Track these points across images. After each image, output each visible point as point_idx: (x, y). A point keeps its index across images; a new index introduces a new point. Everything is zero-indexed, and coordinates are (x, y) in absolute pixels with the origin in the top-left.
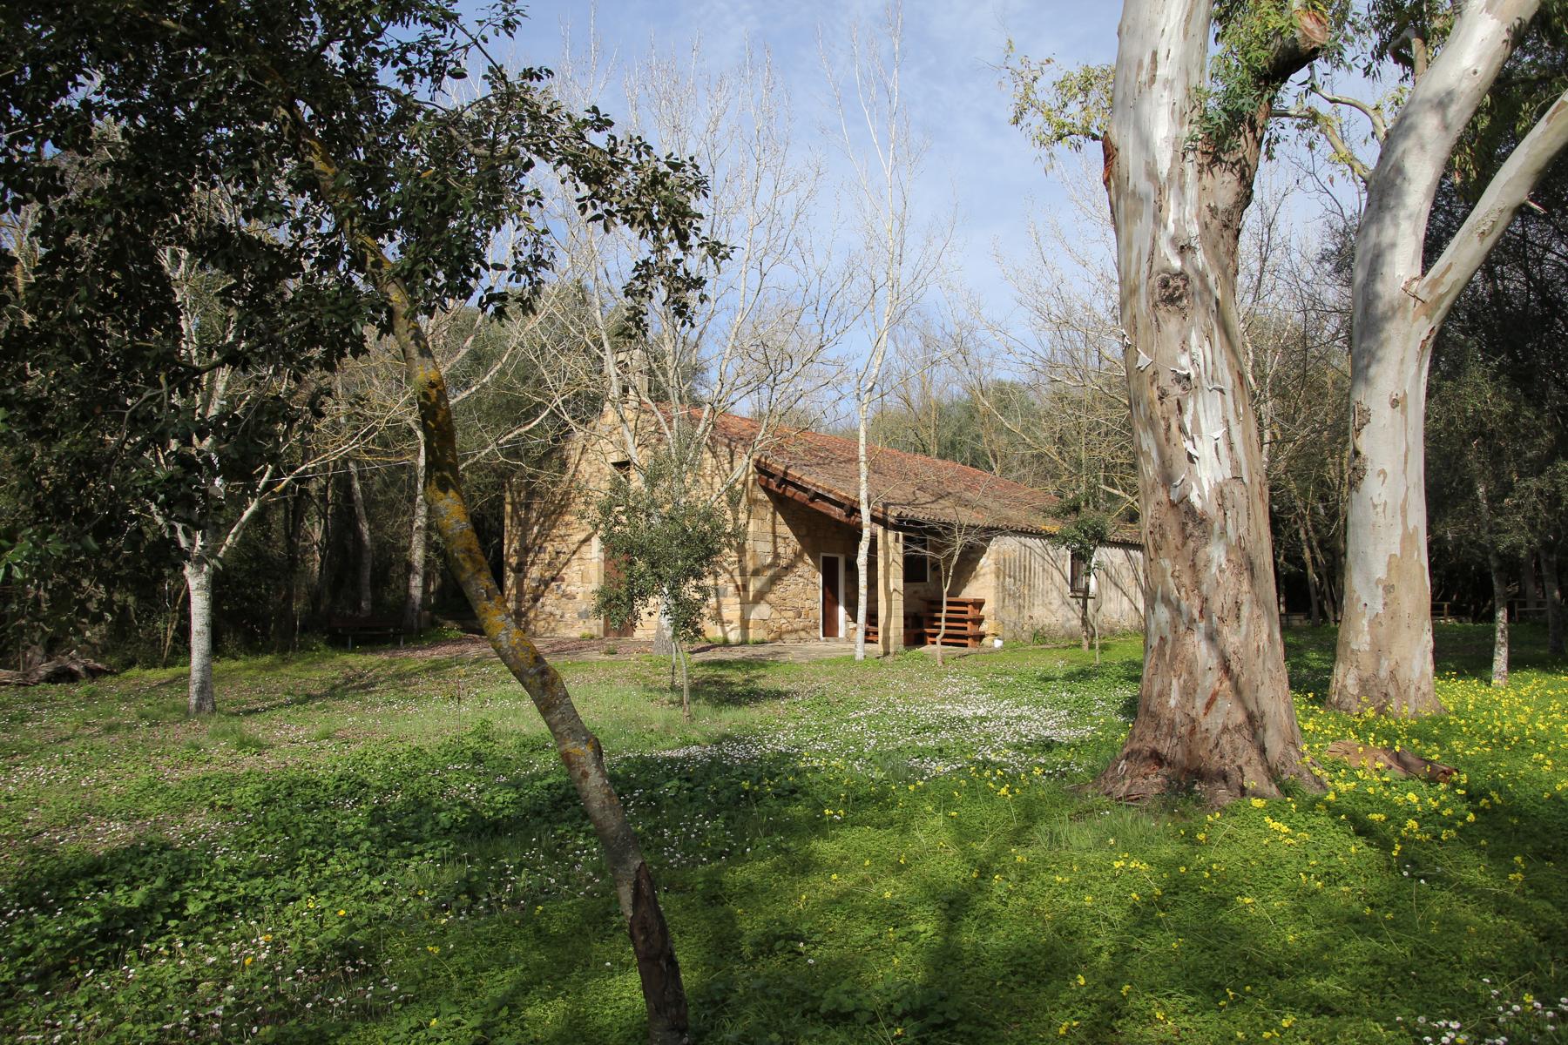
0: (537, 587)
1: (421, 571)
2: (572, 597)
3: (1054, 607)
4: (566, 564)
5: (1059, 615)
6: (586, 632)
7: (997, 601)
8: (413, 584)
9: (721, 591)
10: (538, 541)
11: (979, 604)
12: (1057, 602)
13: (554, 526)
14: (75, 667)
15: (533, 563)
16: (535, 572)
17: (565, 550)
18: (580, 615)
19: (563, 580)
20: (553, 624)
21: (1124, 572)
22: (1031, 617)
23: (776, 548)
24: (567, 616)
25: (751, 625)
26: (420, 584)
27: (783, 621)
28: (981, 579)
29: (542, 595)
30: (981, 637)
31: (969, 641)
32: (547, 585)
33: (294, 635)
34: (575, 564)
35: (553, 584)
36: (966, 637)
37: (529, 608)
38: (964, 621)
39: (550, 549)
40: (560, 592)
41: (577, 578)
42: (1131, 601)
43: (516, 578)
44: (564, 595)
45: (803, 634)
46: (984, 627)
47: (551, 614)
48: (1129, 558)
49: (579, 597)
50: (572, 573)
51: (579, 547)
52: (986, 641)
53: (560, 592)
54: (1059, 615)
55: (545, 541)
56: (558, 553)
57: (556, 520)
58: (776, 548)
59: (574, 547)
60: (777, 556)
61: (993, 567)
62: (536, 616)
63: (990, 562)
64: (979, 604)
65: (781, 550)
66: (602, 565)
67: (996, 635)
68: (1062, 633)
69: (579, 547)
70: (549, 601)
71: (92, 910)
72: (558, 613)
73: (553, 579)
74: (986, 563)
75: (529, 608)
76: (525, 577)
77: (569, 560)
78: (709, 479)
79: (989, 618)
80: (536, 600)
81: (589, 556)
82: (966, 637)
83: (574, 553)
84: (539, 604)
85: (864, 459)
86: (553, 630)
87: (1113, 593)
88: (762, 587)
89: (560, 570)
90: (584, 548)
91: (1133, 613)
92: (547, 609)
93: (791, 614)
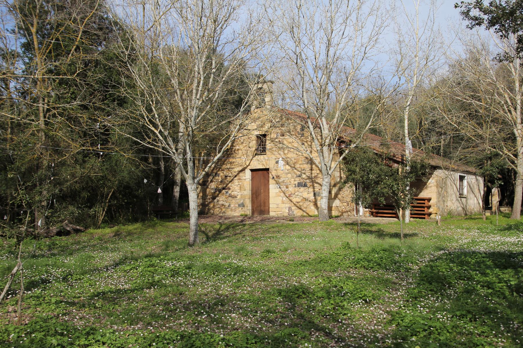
0: (215, 192)
1: (179, 184)
2: (235, 197)
3: (454, 202)
4: (231, 181)
5: (455, 205)
6: (243, 213)
7: (437, 198)
8: (176, 190)
9: (317, 194)
10: (215, 171)
11: (429, 200)
12: (455, 199)
13: (223, 164)
14: (68, 229)
15: (212, 181)
16: (213, 185)
17: (230, 175)
18: (239, 205)
19: (230, 189)
20: (224, 210)
21: (475, 186)
22: (447, 206)
23: (340, 174)
24: (232, 206)
25: (333, 208)
26: (179, 191)
27: (344, 207)
28: (429, 189)
29: (218, 196)
30: (430, 214)
31: (426, 216)
32: (220, 191)
33: (375, 209)
34: (236, 181)
35: (224, 191)
36: (424, 215)
37: (210, 203)
38: (424, 207)
39: (222, 174)
40: (228, 194)
41: (237, 188)
42: (477, 199)
43: (202, 188)
44: (230, 196)
45: (349, 213)
46: (431, 210)
47: (223, 205)
48: (477, 180)
49: (239, 197)
50: (235, 187)
51: (238, 174)
52: (432, 216)
53: (228, 194)
54: (455, 205)
55: (219, 171)
56: (226, 176)
57: (225, 161)
58: (340, 174)
59: (235, 174)
60: (341, 178)
61: (435, 184)
62: (214, 206)
63: (433, 181)
64: (429, 200)
65: (342, 175)
66: (251, 182)
67: (436, 214)
68: (456, 213)
69: (238, 174)
70: (221, 199)
71: (500, 274)
72: (227, 204)
73: (224, 189)
74: (432, 182)
75: (210, 203)
76: (207, 187)
77: (232, 180)
78: (310, 143)
79: (434, 206)
80: (214, 198)
81: (244, 178)
82: (424, 215)
83: (236, 176)
84: (216, 200)
85: (407, 136)
86: (224, 212)
87: (472, 196)
88: (337, 192)
89: (228, 184)
90: (241, 174)
91: (478, 205)
92: (221, 203)
93: (345, 204)
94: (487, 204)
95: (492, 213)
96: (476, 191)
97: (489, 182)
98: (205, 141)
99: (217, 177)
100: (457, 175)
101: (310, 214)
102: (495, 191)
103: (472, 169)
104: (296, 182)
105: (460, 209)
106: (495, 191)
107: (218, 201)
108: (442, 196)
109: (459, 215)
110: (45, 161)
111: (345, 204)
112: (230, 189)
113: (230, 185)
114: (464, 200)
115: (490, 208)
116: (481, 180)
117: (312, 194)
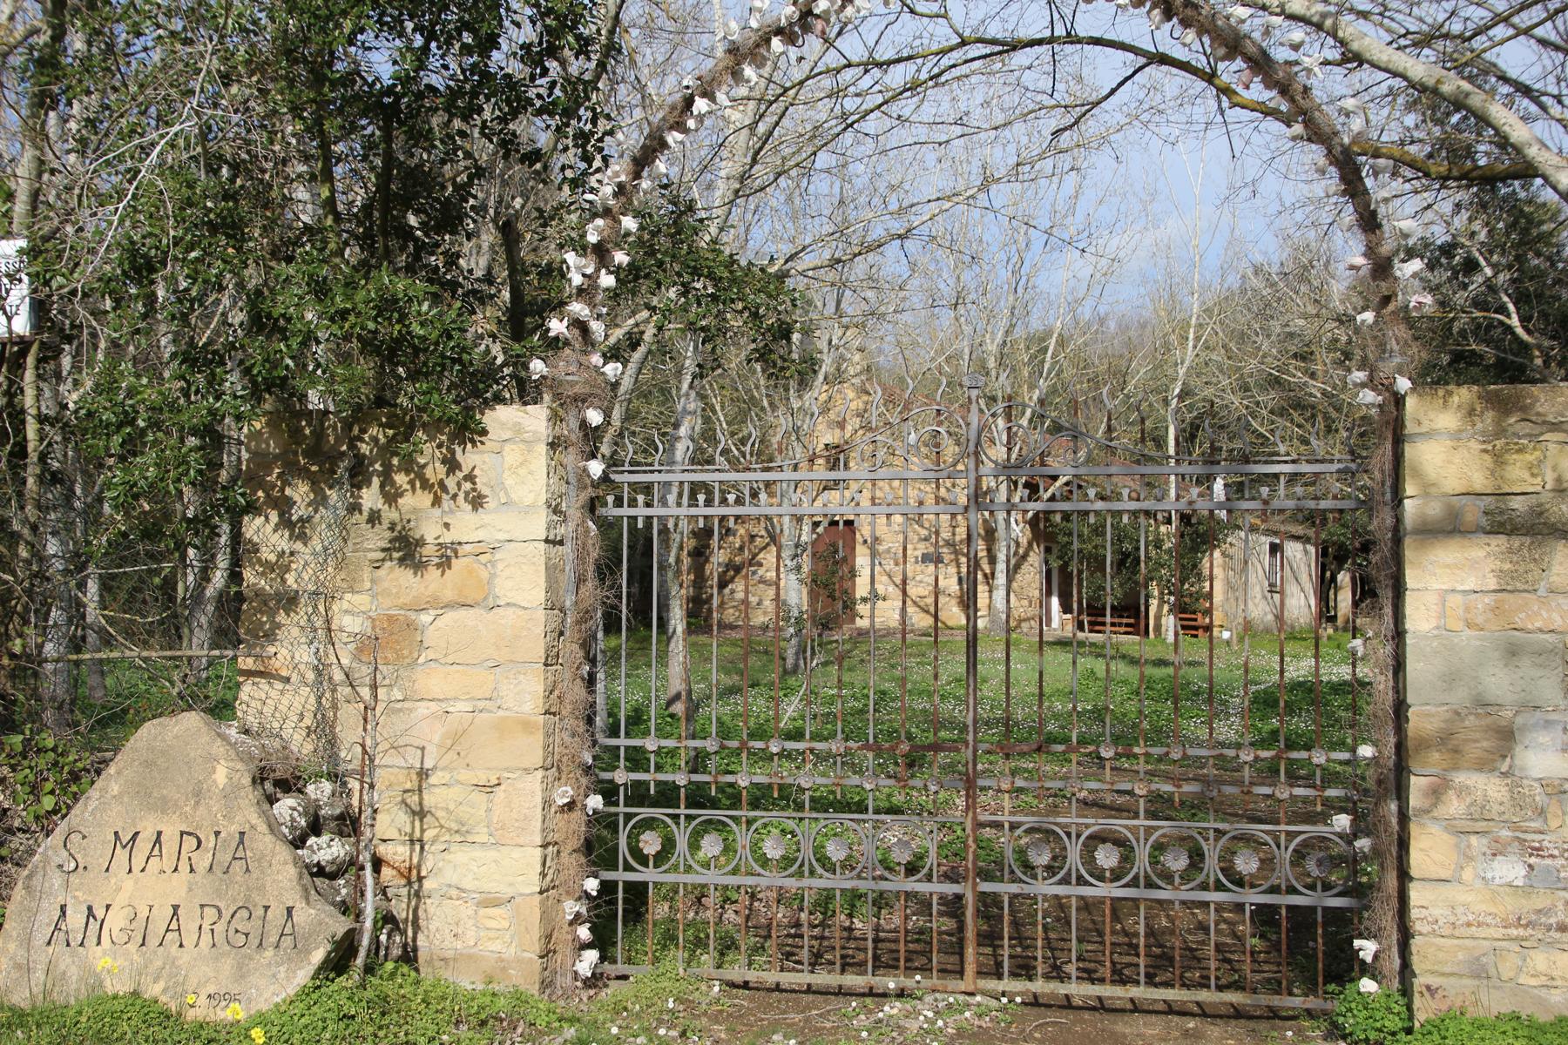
0: (725, 572)
19: (761, 565)
29: (732, 580)
31: (1200, 632)
36: (1196, 628)
39: (742, 531)
76: (707, 560)
82: (1196, 628)
94: (1326, 613)
95: (1336, 629)
96: (1304, 578)
97: (1331, 558)
98: (462, 134)
99: (731, 538)
100: (1266, 541)
101: (950, 624)
102: (1344, 578)
103: (1299, 530)
104: (919, 553)
105: (1270, 617)
106: (1344, 578)
107: (732, 592)
108: (1238, 589)
109: (1267, 631)
110: (666, 908)
111: (1025, 603)
112: (761, 565)
113: (761, 555)
114: (1277, 597)
115: (1333, 619)
116: (1312, 549)
117: (955, 579)
